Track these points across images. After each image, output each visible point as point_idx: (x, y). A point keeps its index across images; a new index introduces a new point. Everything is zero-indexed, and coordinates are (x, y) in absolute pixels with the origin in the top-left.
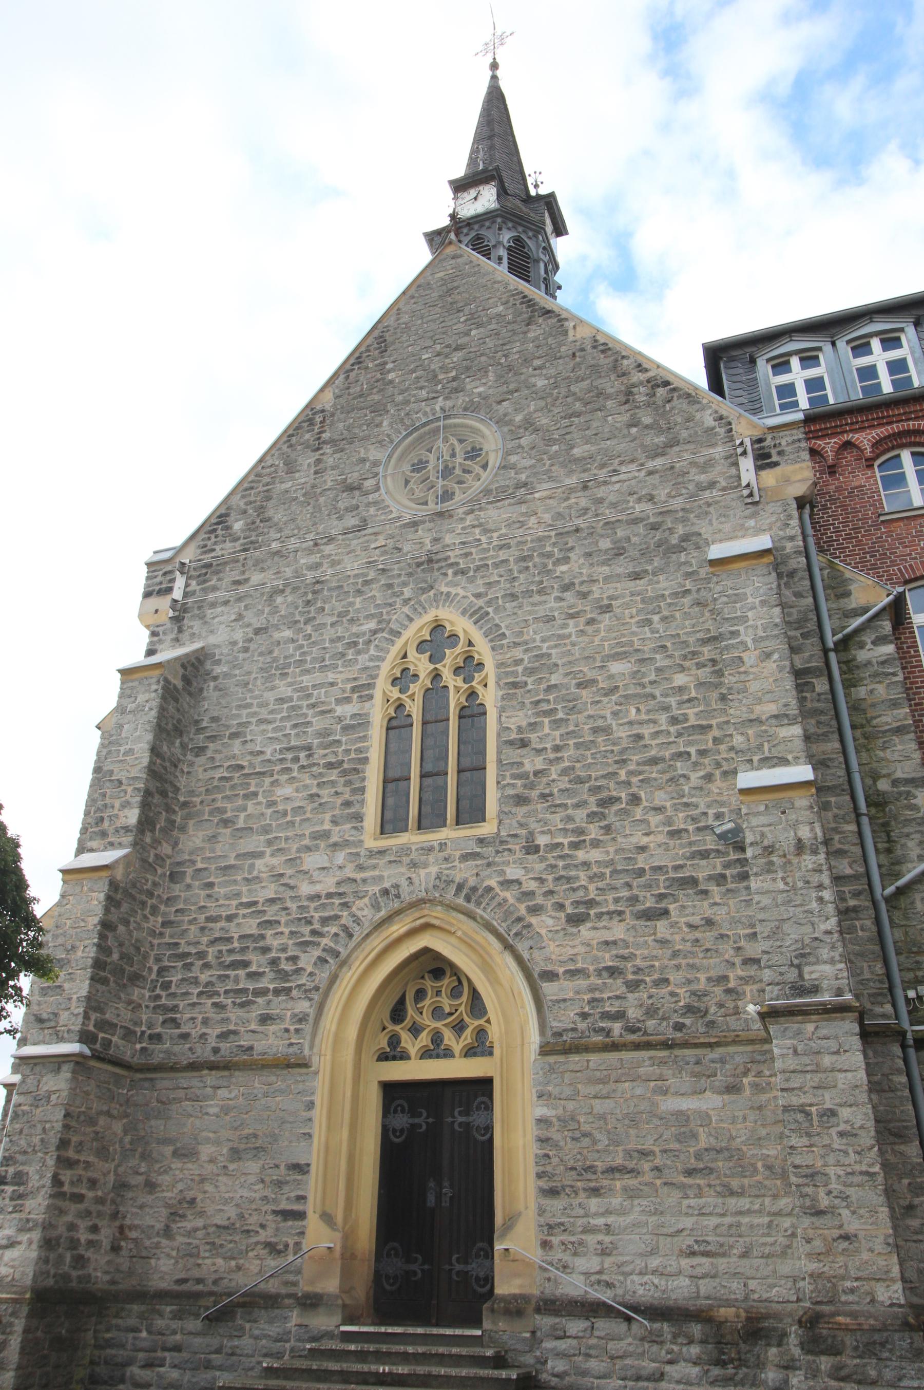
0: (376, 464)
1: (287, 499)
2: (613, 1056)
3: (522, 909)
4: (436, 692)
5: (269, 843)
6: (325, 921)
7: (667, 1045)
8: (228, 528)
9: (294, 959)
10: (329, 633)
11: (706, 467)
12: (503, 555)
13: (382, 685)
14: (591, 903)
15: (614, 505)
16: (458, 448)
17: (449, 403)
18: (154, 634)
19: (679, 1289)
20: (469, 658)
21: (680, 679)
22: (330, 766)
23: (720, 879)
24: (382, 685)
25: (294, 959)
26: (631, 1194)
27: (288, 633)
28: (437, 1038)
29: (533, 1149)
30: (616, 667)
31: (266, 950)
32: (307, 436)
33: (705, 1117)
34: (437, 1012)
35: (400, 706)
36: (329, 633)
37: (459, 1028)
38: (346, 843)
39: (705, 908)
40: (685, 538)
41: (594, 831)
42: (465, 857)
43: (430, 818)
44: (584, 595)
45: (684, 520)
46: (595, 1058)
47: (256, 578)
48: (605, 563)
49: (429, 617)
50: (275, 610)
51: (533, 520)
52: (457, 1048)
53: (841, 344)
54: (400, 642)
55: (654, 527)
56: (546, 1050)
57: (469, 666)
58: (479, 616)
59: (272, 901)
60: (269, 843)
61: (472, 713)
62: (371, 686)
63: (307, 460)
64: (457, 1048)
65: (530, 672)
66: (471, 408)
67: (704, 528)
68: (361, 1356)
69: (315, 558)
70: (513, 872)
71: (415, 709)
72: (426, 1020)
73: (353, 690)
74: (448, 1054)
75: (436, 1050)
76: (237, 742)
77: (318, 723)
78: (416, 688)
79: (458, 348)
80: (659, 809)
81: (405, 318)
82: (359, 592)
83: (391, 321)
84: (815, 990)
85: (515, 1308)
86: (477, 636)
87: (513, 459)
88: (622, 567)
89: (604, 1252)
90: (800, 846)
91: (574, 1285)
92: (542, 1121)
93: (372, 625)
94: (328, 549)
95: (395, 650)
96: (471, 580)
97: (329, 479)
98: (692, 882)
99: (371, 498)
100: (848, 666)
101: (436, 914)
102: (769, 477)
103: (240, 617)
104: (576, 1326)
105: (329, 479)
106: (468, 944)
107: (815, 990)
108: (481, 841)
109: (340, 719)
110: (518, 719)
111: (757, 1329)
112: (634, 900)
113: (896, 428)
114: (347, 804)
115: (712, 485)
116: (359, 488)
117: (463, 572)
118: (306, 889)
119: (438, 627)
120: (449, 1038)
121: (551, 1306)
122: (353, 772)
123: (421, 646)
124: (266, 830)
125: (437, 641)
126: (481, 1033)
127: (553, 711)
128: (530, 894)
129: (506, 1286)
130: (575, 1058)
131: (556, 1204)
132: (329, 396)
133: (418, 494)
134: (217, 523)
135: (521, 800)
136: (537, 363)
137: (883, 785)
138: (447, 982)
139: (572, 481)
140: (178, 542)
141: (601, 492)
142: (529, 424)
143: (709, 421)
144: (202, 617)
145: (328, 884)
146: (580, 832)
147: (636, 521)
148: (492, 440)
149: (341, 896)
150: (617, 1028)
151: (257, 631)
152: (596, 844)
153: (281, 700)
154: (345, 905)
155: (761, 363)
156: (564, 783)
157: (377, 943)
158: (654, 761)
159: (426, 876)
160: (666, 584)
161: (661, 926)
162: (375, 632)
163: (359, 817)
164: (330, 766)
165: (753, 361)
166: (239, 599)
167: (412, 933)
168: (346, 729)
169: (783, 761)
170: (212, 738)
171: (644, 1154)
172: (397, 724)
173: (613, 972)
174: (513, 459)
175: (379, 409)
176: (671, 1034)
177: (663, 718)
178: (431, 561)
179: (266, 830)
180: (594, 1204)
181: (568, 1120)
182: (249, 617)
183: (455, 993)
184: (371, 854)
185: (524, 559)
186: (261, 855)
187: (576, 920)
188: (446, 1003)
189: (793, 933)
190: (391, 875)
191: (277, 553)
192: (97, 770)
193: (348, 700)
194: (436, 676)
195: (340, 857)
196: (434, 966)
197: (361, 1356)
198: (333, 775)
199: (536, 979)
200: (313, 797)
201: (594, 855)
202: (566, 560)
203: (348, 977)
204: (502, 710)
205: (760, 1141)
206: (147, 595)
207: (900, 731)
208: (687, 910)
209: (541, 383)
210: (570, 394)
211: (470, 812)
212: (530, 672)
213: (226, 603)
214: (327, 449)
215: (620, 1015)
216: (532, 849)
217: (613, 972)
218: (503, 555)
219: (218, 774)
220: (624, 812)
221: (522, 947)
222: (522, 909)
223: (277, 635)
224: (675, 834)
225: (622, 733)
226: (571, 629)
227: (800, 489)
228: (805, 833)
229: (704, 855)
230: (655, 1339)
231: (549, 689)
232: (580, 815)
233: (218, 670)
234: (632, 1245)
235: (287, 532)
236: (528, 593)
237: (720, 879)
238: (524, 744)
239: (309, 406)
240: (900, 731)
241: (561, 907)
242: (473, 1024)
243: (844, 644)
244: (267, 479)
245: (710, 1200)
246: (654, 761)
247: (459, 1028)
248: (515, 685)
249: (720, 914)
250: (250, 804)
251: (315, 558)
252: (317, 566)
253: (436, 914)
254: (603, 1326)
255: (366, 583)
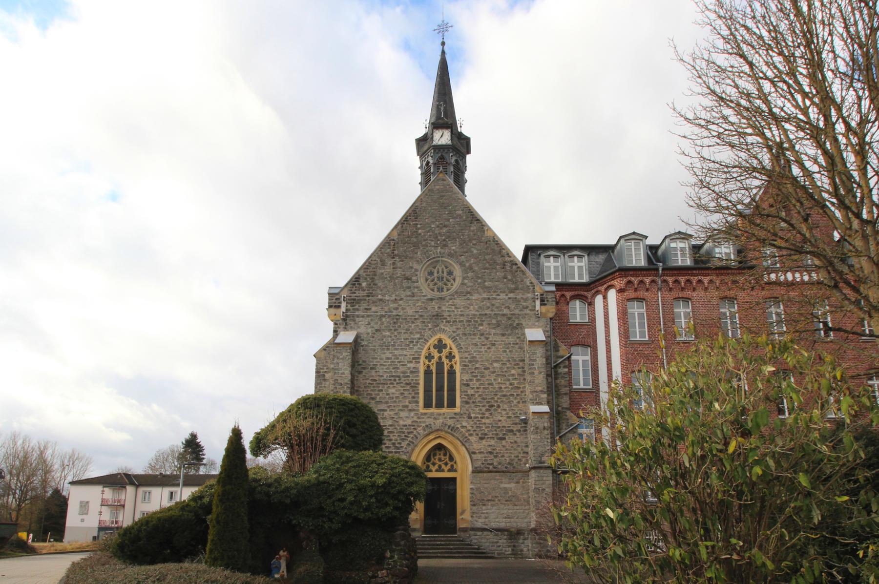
0: (416, 270)
1: (382, 277)
2: (489, 474)
3: (467, 434)
4: (440, 365)
5: (389, 407)
6: (409, 433)
7: (503, 472)
8: (360, 284)
9: (400, 443)
10: (403, 336)
11: (526, 300)
12: (462, 319)
13: (422, 359)
14: (486, 434)
15: (497, 308)
16: (445, 270)
17: (442, 251)
18: (335, 324)
19: (502, 525)
20: (450, 353)
21: (513, 372)
22: (407, 384)
23: (519, 431)
24: (422, 359)
25: (400, 443)
26: (493, 505)
27: (388, 333)
28: (440, 466)
29: (469, 495)
30: (495, 365)
31: (391, 440)
32: (388, 250)
33: (511, 489)
34: (440, 460)
35: (428, 367)
36: (403, 336)
37: (446, 464)
38: (414, 410)
39: (515, 438)
40: (518, 324)
41: (487, 414)
42: (450, 418)
43: (440, 405)
44: (487, 339)
45: (518, 318)
46: (485, 474)
47: (374, 309)
48: (494, 328)
49: (437, 337)
50: (382, 323)
51: (472, 307)
52: (446, 469)
53: (566, 256)
54: (428, 344)
55: (509, 319)
56: (473, 472)
57: (450, 357)
58: (454, 340)
59: (391, 425)
60: (389, 407)
61: (452, 373)
62: (419, 358)
63: (389, 262)
64: (446, 469)
65: (470, 362)
66: (450, 255)
67: (524, 324)
68: (431, 541)
69: (396, 305)
70: (464, 424)
71: (433, 369)
72: (437, 461)
73: (413, 359)
74: (443, 471)
75: (440, 470)
76: (373, 371)
77: (402, 369)
78: (434, 361)
79: (445, 226)
80: (505, 410)
81: (424, 204)
82: (413, 323)
83: (418, 204)
84: (544, 463)
85: (465, 530)
86: (453, 347)
87: (466, 281)
88: (499, 331)
89: (486, 518)
90: (544, 428)
91: (479, 525)
92: (472, 489)
93: (418, 336)
94: (401, 302)
95: (426, 347)
96: (452, 326)
97: (399, 272)
98: (512, 431)
99: (415, 284)
100: (556, 373)
101: (443, 434)
102: (544, 309)
103: (369, 324)
104: (479, 533)
105: (399, 272)
106: (451, 442)
107: (544, 463)
108: (455, 414)
109: (409, 368)
110: (466, 377)
111: (519, 532)
112: (497, 434)
113: (577, 293)
114: (413, 397)
115: (527, 307)
116: (410, 279)
117: (449, 322)
118: (401, 423)
119: (440, 341)
120: (443, 467)
121: (473, 529)
122: (415, 387)
123: (435, 347)
124: (387, 403)
125: (440, 346)
126: (452, 466)
127: (476, 376)
128: (469, 431)
129: (461, 525)
130: (481, 474)
131: (474, 508)
132: (395, 233)
133: (431, 286)
134: (356, 281)
135: (467, 403)
136: (474, 242)
137: (560, 409)
138: (442, 452)
139: (485, 295)
140: (342, 285)
141: (494, 302)
142: (471, 268)
143: (528, 284)
144: (354, 321)
145: (409, 422)
146: (483, 414)
147: (504, 315)
148: (458, 271)
149: (414, 425)
150: (491, 467)
151: (377, 330)
152: (488, 418)
153: (388, 358)
154: (415, 429)
155: (542, 256)
156: (479, 399)
157: (425, 440)
158: (504, 396)
159: (439, 422)
160: (511, 339)
161: (504, 442)
162: (419, 339)
163: (417, 402)
164: (407, 384)
165: (539, 255)
166: (368, 316)
167: (434, 439)
168: (411, 372)
169: (541, 404)
170: (364, 368)
171: (496, 497)
172: (428, 373)
173: (491, 453)
174: (466, 281)
175: (416, 246)
176: (504, 469)
177: (508, 383)
178: (438, 316)
179: (387, 403)
180: (484, 507)
181: (478, 489)
182: (373, 324)
183: (445, 455)
184: (422, 414)
185: (470, 321)
186: (386, 410)
187: (481, 439)
188: (443, 458)
189: (540, 449)
190: (429, 421)
191: (381, 300)
192: (317, 372)
193: (411, 362)
194: (440, 358)
195: (412, 414)
196: (440, 447)
197: (431, 541)
198: (408, 387)
199: (471, 453)
200: (402, 394)
201: (487, 421)
202: (482, 325)
203: (417, 450)
204: (461, 373)
205: (522, 494)
206: (330, 306)
207: (566, 394)
208: (510, 438)
209: (475, 252)
210: (485, 259)
211: (452, 404)
212: (470, 362)
213: (363, 317)
214: (397, 258)
215: (492, 464)
216: (470, 418)
217: (491, 453)
218: (462, 319)
219: (368, 381)
220: (496, 410)
221: (467, 445)
222: (467, 434)
223: (384, 333)
224: (509, 417)
225: (497, 386)
226: (482, 350)
227: (551, 315)
228: (546, 425)
229: (516, 424)
230: (497, 535)
231: (476, 368)
232: (484, 409)
233: (363, 343)
234: (492, 516)
235: (384, 292)
236: (470, 334)
237: (519, 431)
238: (468, 385)
239: (388, 236)
240: (566, 394)
241: (477, 435)
242: (450, 464)
243: (556, 367)
244: (373, 266)
245: (511, 507)
246: (504, 396)
247: (446, 464)
248: (465, 366)
249: (518, 440)
250: (381, 393)
251: (396, 305)
252: (396, 309)
253: (443, 434)
254: (485, 533)
255: (416, 319)
